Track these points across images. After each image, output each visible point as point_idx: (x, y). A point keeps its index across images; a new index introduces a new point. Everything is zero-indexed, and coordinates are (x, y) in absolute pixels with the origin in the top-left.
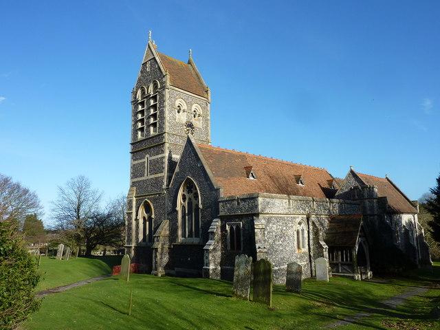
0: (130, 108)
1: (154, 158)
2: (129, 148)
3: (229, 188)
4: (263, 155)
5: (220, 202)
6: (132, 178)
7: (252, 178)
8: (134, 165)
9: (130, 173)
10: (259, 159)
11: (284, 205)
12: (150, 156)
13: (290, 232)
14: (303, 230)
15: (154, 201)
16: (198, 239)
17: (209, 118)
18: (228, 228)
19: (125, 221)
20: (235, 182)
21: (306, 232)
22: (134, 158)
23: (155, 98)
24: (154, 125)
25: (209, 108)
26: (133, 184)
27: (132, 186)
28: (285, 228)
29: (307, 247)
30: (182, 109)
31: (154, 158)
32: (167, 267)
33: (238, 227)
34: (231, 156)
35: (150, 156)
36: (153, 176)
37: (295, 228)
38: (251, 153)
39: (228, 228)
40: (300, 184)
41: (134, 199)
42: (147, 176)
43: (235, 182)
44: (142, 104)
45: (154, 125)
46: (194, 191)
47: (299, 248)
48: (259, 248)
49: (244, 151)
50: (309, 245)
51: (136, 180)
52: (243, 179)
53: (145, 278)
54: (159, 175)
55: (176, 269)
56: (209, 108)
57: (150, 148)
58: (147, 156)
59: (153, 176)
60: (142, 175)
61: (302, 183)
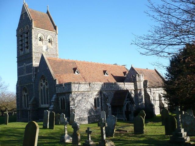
1: (28, 65)
2: (16, 60)
3: (61, 78)
4: (86, 61)
7: (77, 74)
8: (20, 68)
10: (84, 63)
11: (87, 87)
12: (26, 64)
16: (48, 105)
17: (57, 42)
19: (170, 137)
20: (66, 76)
23: (27, 33)
25: (57, 37)
29: (100, 106)
31: (28, 65)
32: (65, 134)
33: (64, 98)
34: (67, 63)
35: (26, 64)
38: (79, 60)
40: (106, 75)
41: (28, 84)
43: (66, 76)
49: (74, 59)
50: (101, 105)
52: (72, 74)
54: (30, 74)
56: (57, 37)
58: (25, 64)
61: (107, 74)
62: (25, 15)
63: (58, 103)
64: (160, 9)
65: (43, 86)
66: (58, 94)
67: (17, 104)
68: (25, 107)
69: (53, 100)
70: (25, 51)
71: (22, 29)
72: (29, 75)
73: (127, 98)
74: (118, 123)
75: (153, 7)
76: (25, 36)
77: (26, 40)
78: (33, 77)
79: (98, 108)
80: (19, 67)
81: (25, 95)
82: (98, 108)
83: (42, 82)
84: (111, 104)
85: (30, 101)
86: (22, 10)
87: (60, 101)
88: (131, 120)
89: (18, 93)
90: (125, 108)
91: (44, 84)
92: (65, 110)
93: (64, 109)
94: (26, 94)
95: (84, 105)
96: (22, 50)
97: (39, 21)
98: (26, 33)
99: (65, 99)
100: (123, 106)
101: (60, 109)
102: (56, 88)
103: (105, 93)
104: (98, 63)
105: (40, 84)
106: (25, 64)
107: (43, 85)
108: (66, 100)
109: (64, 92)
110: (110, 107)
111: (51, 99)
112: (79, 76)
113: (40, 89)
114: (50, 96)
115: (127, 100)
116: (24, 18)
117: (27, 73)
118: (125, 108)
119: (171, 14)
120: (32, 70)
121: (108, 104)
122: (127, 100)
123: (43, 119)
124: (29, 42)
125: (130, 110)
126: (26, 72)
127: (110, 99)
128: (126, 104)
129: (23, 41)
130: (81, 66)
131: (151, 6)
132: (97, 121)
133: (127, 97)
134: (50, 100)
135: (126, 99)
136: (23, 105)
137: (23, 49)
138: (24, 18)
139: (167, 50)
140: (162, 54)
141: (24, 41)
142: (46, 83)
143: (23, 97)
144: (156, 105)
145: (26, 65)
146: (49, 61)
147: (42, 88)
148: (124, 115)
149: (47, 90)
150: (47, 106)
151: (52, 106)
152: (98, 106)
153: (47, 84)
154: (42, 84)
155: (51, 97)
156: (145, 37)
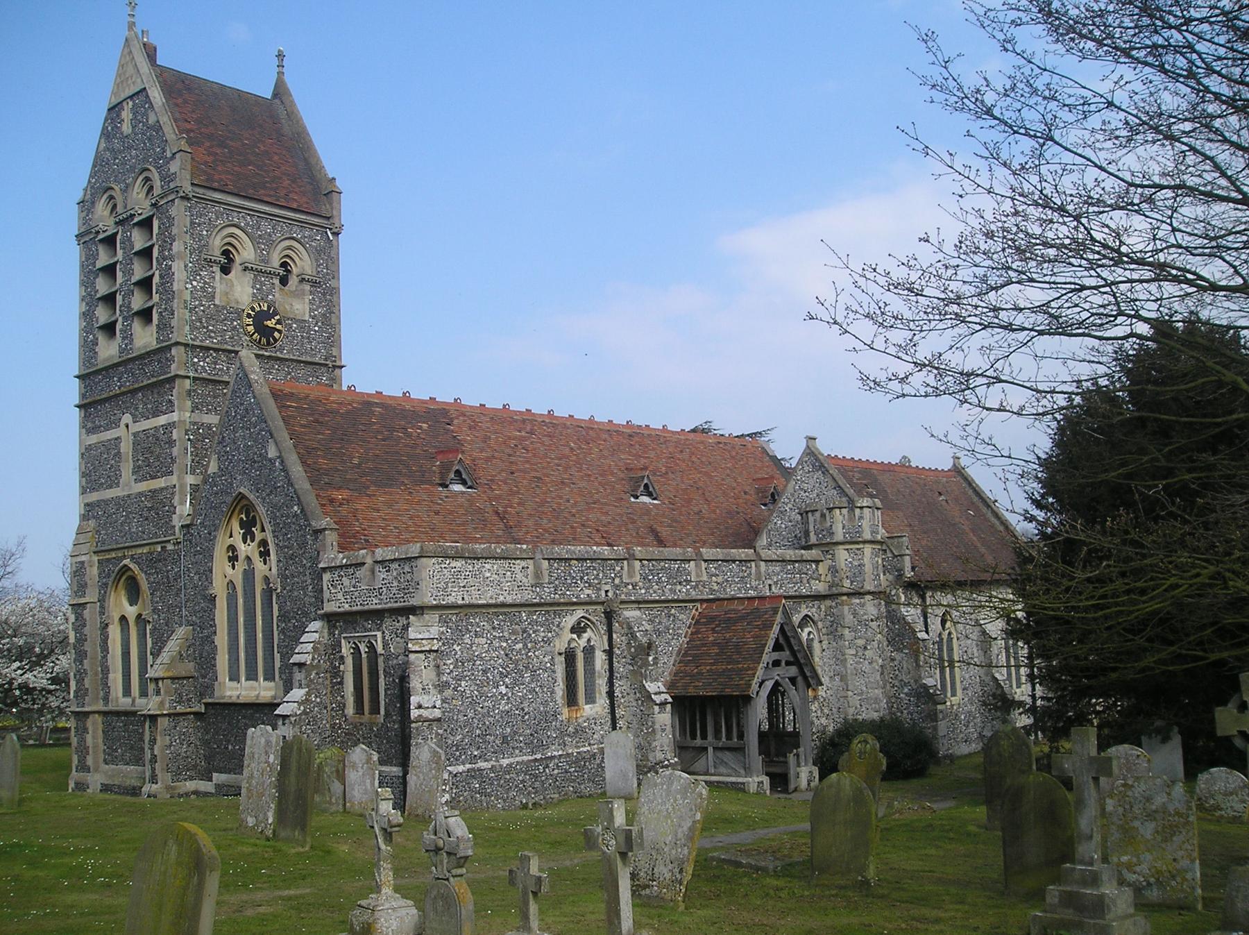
0: (73, 254)
2: (72, 391)
5: (324, 569)
6: (84, 491)
8: (89, 448)
9: (313, 139)
11: (519, 576)
13: (540, 657)
14: (589, 651)
15: (151, 563)
16: (272, 684)
18: (346, 650)
21: (600, 659)
22: (89, 426)
23: (146, 224)
24: (145, 315)
26: (89, 511)
27: (84, 518)
28: (520, 646)
29: (602, 701)
30: (238, 259)
36: (144, 486)
37: (561, 645)
39: (346, 650)
42: (129, 485)
44: (110, 241)
45: (145, 315)
46: (259, 536)
47: (571, 700)
48: (420, 707)
50: (611, 694)
51: (94, 497)
53: (99, 787)
55: (215, 775)
57: (133, 392)
58: (127, 418)
59: (144, 486)
60: (113, 482)
61: (650, 495)
62: (135, 111)
63: (336, 673)
64: (990, 98)
65: (241, 566)
66: (331, 619)
67: (1221, 737)
68: (127, 691)
69: (304, 653)
70: (128, 337)
71: (111, 197)
72: (154, 491)
73: (777, 647)
74: (1047, 902)
75: (951, 83)
76: (129, 239)
77: (139, 272)
78: (184, 509)
79: (587, 707)
80: (93, 439)
81: (123, 619)
82: (588, 710)
83: (237, 540)
84: (671, 686)
85: (156, 654)
86: (119, 75)
87: (349, 661)
88: (796, 790)
89: (83, 605)
90: (759, 713)
91: (243, 549)
92: (381, 718)
93: (375, 710)
94: (131, 611)
95: (503, 689)
96: (109, 329)
97: (223, 145)
98: (140, 224)
99: (380, 649)
100: (747, 699)
101: (350, 710)
102: (326, 577)
103: (637, 613)
104: (591, 420)
105: (220, 555)
106: (127, 418)
107: (242, 557)
108: (387, 659)
109: (374, 604)
110: (663, 704)
111: (287, 652)
112: (471, 501)
113: (219, 588)
114: (282, 631)
115: (776, 663)
116: (126, 128)
117: (144, 479)
118: (759, 713)
119: (1057, 138)
120: (173, 460)
121: (651, 687)
122: (776, 663)
123: (238, 768)
124: (156, 280)
125: (790, 729)
126: (137, 470)
127: (666, 660)
128: (769, 685)
129: (119, 274)
130: (486, 439)
131: (936, 74)
132: (401, 727)
133: (771, 643)
134: (285, 656)
135: (768, 656)
136: (116, 678)
137: (119, 326)
138: (126, 128)
139: (1022, 365)
140: (994, 396)
141: (129, 273)
142: (264, 543)
143: (115, 632)
144: (954, 694)
145: (136, 428)
146: (282, 407)
147: (237, 575)
148: (757, 760)
149: (268, 592)
150: (263, 690)
151: (298, 694)
152: (590, 699)
153: (265, 554)
154: (232, 548)
155: (293, 638)
156: (899, 274)
